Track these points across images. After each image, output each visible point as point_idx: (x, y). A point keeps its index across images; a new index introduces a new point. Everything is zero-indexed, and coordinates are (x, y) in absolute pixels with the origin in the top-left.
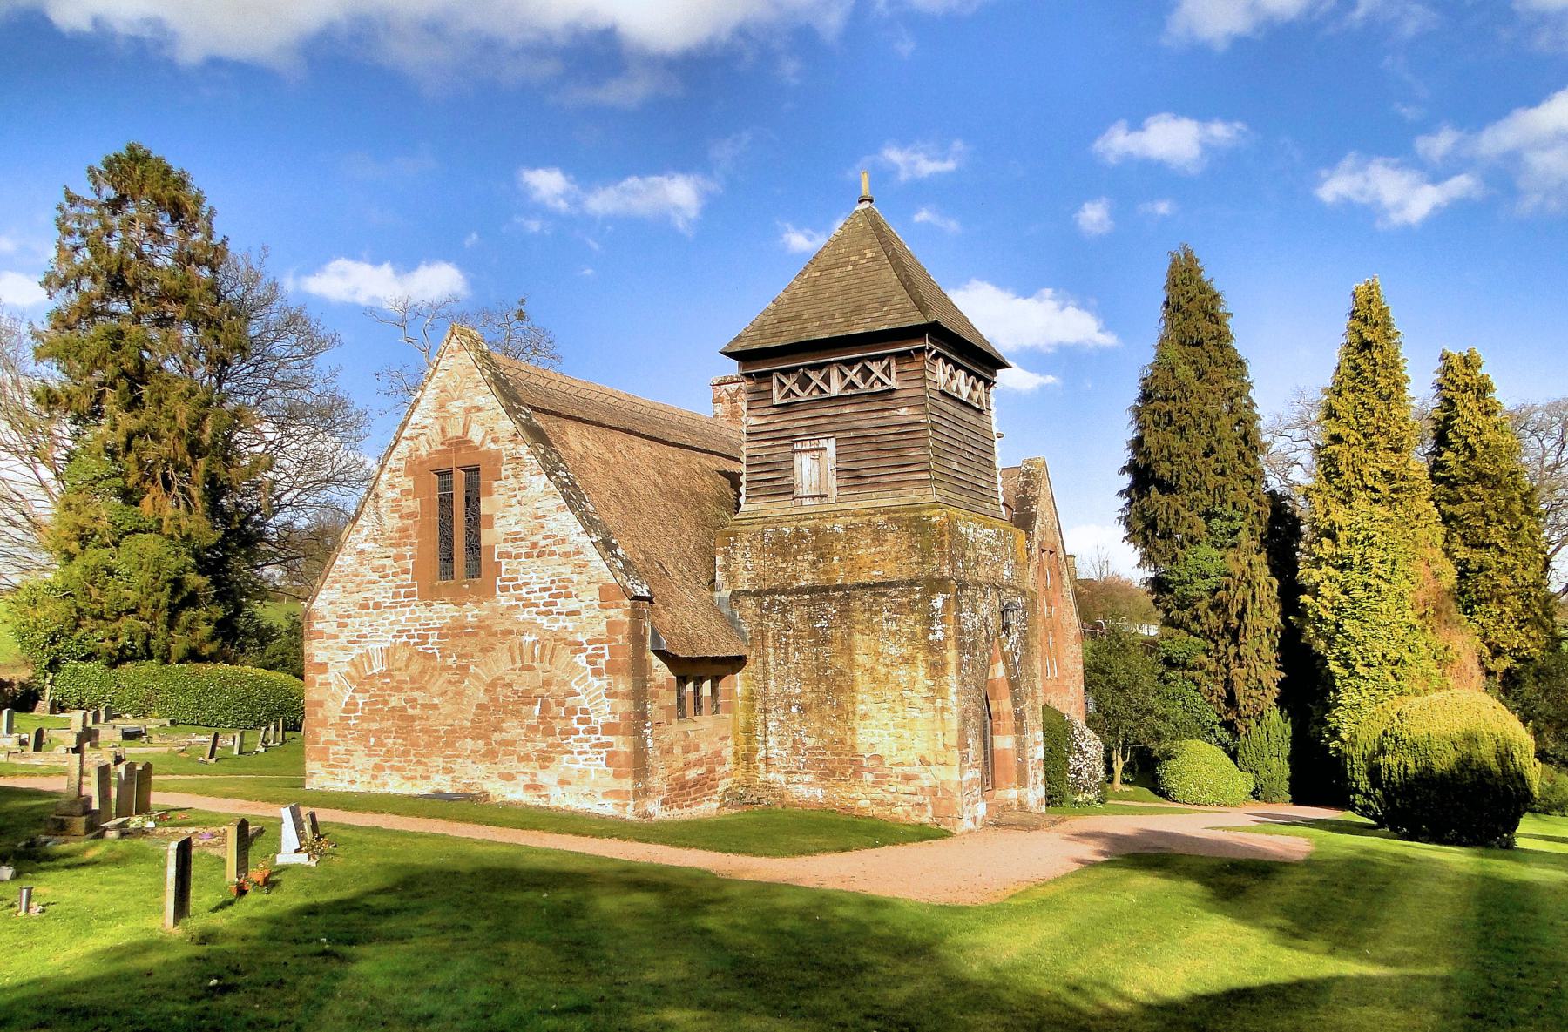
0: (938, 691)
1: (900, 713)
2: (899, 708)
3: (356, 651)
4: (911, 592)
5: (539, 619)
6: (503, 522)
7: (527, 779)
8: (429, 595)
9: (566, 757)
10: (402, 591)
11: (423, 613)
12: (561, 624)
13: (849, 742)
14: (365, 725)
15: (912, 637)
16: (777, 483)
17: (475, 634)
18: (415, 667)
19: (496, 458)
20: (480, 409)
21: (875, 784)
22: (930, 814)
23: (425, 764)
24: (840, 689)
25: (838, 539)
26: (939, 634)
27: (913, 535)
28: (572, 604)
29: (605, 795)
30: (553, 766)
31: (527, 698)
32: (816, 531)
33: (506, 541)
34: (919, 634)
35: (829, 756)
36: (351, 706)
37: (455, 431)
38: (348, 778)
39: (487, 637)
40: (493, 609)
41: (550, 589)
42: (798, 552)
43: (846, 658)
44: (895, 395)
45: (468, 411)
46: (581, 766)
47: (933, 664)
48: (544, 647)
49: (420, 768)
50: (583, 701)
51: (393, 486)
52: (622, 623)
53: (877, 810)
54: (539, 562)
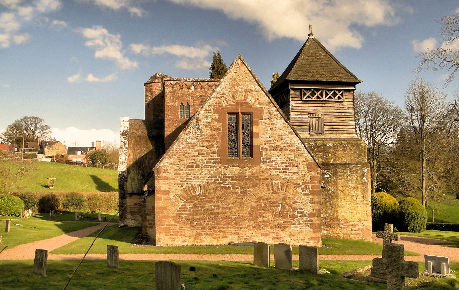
0: (365, 198)
1: (353, 206)
2: (352, 204)
3: (186, 185)
4: (356, 167)
5: (281, 175)
6: (264, 136)
7: (274, 235)
8: (226, 163)
9: (292, 226)
10: (212, 161)
11: (223, 170)
12: (290, 176)
13: (336, 215)
14: (191, 217)
15: (357, 181)
16: (304, 127)
17: (250, 179)
18: (220, 192)
19: (261, 111)
20: (252, 91)
21: (344, 228)
22: (362, 236)
23: (224, 232)
24: (333, 198)
25: (331, 148)
26: (366, 180)
27: (356, 149)
28: (295, 169)
29: (309, 239)
30: (287, 229)
31: (275, 204)
32: (323, 145)
33: (265, 144)
34: (359, 180)
35: (329, 220)
36: (183, 209)
37: (240, 98)
38: (181, 239)
39: (255, 181)
40: (259, 170)
41: (286, 163)
42: (317, 152)
43: (335, 187)
44: (344, 103)
45: (246, 90)
46: (299, 229)
47: (363, 190)
48: (283, 185)
49: (221, 234)
50: (300, 205)
51: (207, 117)
52: (317, 177)
53: (345, 237)
54: (280, 152)
